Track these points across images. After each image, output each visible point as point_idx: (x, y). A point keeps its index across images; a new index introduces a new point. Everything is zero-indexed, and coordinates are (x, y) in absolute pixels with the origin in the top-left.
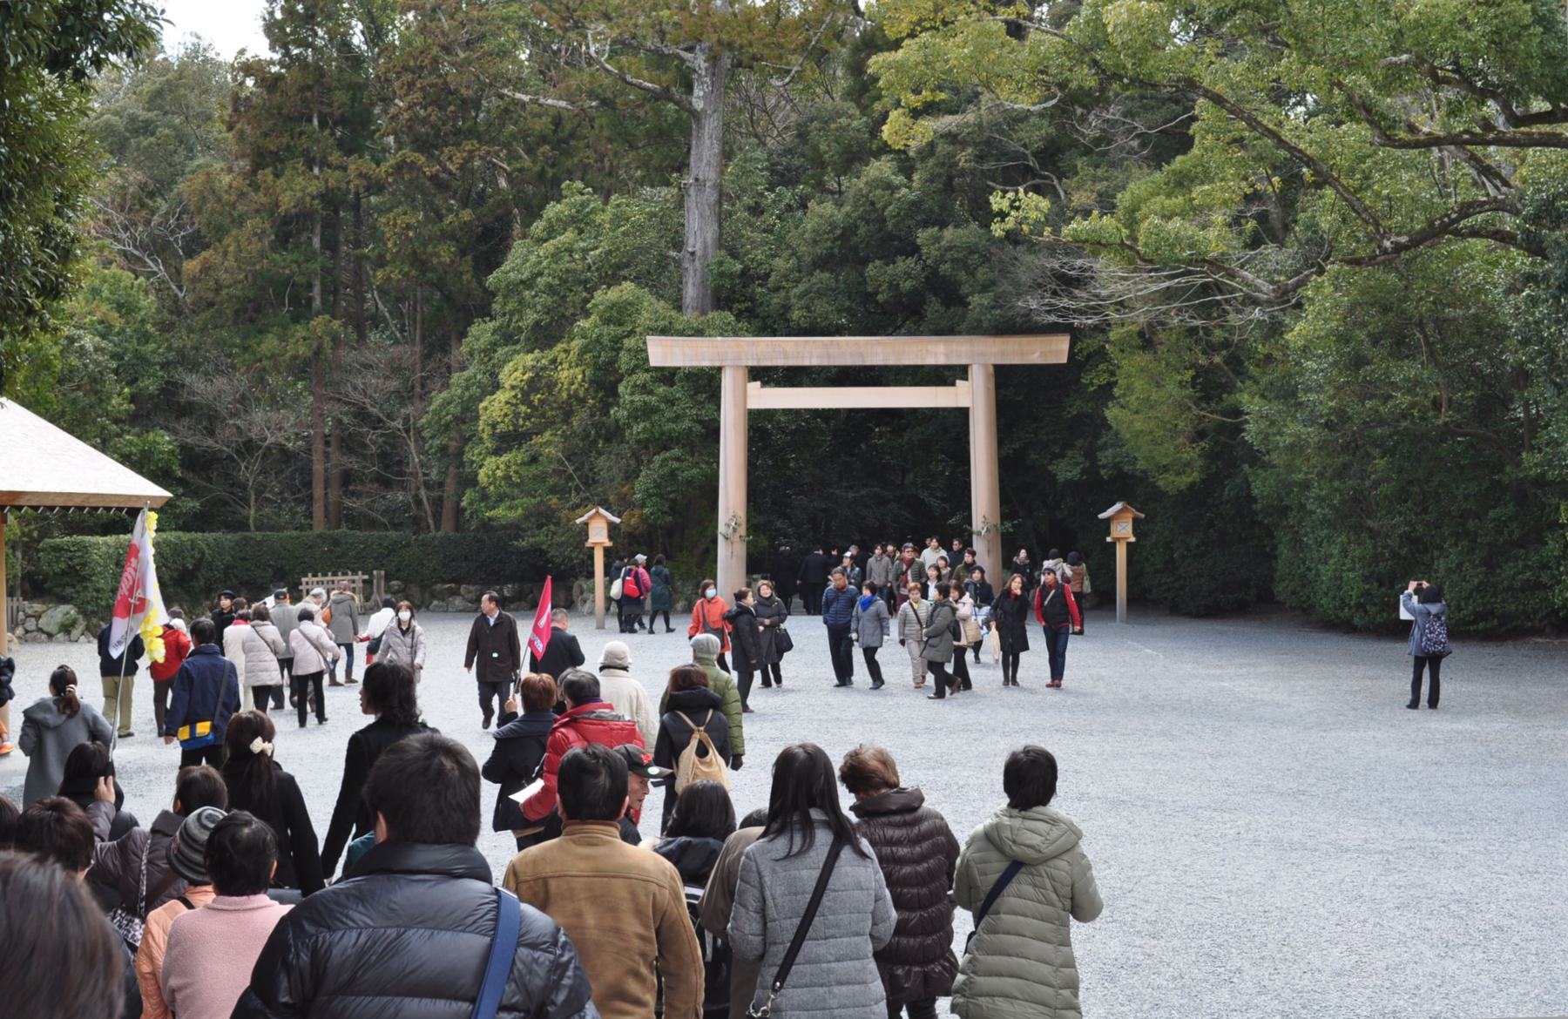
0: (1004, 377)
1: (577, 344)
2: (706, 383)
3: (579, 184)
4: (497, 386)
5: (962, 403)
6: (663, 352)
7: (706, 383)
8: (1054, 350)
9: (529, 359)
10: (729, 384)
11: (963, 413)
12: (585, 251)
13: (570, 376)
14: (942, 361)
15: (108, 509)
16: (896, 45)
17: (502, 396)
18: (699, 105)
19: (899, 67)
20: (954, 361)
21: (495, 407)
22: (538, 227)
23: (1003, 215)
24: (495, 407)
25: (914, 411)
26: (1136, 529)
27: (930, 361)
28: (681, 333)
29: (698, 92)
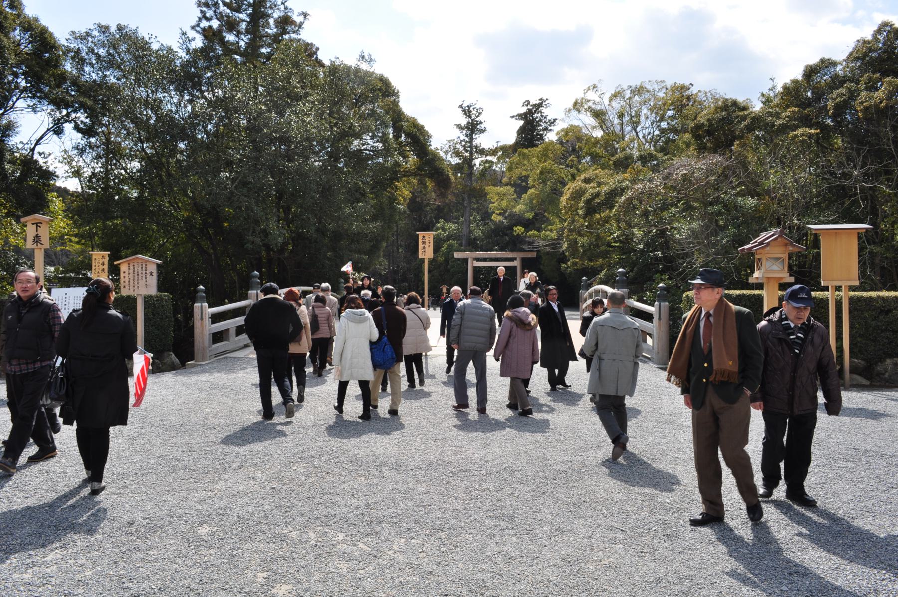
6: (457, 255)
8: (534, 255)
10: (470, 261)
11: (515, 267)
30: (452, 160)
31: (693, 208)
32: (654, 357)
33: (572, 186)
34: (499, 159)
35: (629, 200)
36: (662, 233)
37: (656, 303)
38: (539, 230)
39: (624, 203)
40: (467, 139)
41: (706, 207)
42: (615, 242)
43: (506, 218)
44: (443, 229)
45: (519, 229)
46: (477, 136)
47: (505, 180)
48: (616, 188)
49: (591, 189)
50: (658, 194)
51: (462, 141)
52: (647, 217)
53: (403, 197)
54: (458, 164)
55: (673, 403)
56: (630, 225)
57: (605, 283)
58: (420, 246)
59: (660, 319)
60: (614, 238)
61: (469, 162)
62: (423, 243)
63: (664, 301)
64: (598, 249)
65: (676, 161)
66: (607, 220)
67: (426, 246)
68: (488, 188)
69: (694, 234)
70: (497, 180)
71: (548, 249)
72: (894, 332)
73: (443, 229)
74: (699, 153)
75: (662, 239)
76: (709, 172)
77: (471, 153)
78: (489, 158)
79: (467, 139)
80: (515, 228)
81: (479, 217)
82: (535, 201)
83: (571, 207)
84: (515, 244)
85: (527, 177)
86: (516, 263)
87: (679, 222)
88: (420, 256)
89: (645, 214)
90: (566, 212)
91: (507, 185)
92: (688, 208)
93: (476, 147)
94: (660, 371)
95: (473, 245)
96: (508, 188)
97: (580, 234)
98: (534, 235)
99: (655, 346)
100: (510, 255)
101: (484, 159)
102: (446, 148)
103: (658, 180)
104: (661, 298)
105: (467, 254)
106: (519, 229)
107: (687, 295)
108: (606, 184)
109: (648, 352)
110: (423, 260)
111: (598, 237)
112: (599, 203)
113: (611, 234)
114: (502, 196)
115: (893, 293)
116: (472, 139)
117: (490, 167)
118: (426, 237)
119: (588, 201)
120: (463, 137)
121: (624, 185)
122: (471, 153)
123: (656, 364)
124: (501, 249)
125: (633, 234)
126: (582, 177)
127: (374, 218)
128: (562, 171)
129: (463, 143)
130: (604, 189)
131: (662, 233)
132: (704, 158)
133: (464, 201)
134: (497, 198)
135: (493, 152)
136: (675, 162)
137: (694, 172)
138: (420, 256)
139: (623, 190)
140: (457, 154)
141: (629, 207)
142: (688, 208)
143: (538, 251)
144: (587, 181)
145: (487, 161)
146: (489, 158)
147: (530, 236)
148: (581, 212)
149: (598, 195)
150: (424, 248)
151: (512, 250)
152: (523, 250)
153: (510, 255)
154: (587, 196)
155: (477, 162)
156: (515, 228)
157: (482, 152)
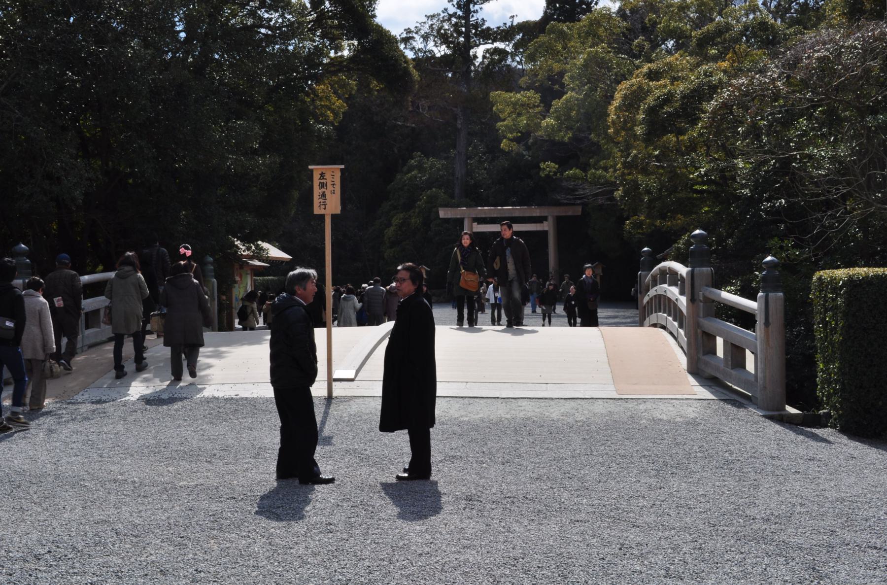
0: (560, 221)
1: (417, 210)
2: (459, 222)
3: (419, 153)
4: (391, 225)
5: (546, 229)
6: (443, 213)
7: (459, 222)
8: (578, 211)
9: (401, 215)
10: (466, 223)
11: (545, 233)
12: (421, 178)
13: (415, 221)
14: (538, 215)
15: (786, 333)
16: (504, 120)
17: (392, 228)
18: (459, 126)
19: (506, 126)
20: (543, 215)
21: (390, 232)
22: (405, 169)
23: (544, 169)
24: (390, 232)
25: (324, 266)
26: (603, 271)
27: (534, 215)
28: (451, 207)
29: (459, 122)
30: (435, 50)
31: (841, 120)
32: (758, 395)
33: (623, 88)
34: (516, 47)
35: (726, 106)
36: (785, 164)
37: (760, 294)
38: (585, 168)
39: (714, 112)
40: (460, 13)
41: (863, 118)
42: (703, 183)
43: (528, 148)
44: (420, 167)
45: (548, 167)
46: (477, 7)
47: (523, 81)
48: (700, 86)
49: (659, 88)
50: (776, 96)
51: (451, 16)
52: (758, 137)
53: (333, 111)
54: (445, 56)
55: (778, 493)
56: (731, 154)
57: (676, 259)
58: (317, 191)
59: (767, 323)
60: (700, 176)
61: (462, 54)
62: (322, 185)
63: (775, 290)
64: (678, 199)
65: (809, 36)
66: (692, 147)
67: (328, 193)
68: (493, 94)
69: (842, 168)
70: (506, 79)
71: (600, 201)
72: (480, 583)
73: (420, 167)
74: (850, 20)
75: (785, 175)
76: (868, 52)
77: (467, 37)
78: (500, 45)
79: (460, 13)
80: (542, 165)
81: (481, 148)
82: (573, 113)
83: (625, 122)
84: (538, 192)
85: (561, 74)
86: (545, 226)
87: (817, 146)
88: (317, 211)
89: (754, 132)
90: (617, 132)
91: (528, 89)
92: (832, 120)
93: (476, 26)
94: (768, 423)
95: (474, 197)
96: (530, 93)
97: (645, 171)
98: (575, 178)
99: (760, 375)
100: (536, 212)
101: (489, 46)
102: (425, 29)
103: (774, 70)
104: (769, 284)
105: (461, 212)
106: (548, 167)
107: (820, 279)
108: (684, 79)
109: (746, 384)
110: (322, 217)
111: (673, 175)
112: (670, 114)
113: (697, 168)
114: (518, 108)
115: (880, 271)
116: (467, 13)
117: (500, 61)
118: (328, 176)
119: (652, 111)
120: (452, 10)
121: (715, 79)
122: (467, 37)
123: (759, 407)
124: (522, 202)
125: (735, 167)
126: (645, 69)
127: (267, 147)
128: (616, 60)
129: (454, 20)
130: (681, 88)
131: (785, 164)
132: (859, 28)
133: (456, 119)
134: (508, 110)
135: (506, 34)
136: (806, 37)
137: (840, 53)
138: (317, 211)
139: (714, 89)
140: (444, 38)
141: (726, 116)
142: (832, 120)
143: (584, 205)
144: (653, 75)
145: (496, 51)
146: (500, 45)
147: (569, 178)
148: (639, 130)
149: (668, 99)
150: (323, 195)
151: (540, 204)
152: (558, 204)
153: (536, 212)
154: (650, 100)
155: (479, 51)
156: (542, 165)
157: (488, 35)
